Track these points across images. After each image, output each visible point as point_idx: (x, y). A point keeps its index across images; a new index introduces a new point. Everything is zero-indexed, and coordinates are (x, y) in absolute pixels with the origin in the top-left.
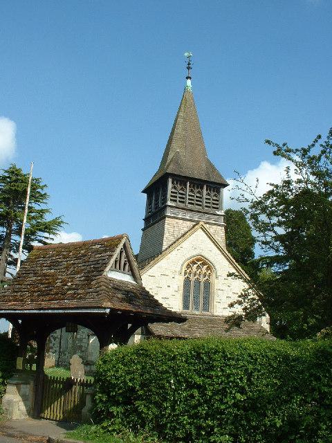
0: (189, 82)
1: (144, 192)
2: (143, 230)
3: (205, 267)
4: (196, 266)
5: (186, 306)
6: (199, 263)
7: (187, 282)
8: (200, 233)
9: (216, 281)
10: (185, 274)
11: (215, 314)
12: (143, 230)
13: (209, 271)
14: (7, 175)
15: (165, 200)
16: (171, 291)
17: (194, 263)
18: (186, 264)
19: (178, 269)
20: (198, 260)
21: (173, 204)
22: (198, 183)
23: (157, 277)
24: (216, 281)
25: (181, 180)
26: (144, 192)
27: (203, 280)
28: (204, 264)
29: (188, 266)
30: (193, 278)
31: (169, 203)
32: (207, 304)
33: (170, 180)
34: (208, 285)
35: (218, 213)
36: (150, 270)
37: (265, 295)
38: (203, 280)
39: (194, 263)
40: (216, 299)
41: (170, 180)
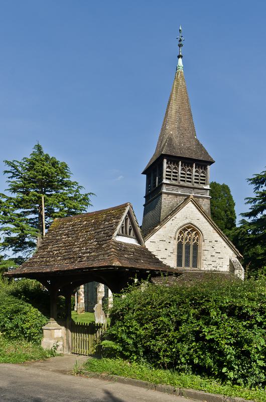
0: (180, 60)
19: (173, 236)
20: (189, 228)
22: (188, 162)
39: (185, 230)
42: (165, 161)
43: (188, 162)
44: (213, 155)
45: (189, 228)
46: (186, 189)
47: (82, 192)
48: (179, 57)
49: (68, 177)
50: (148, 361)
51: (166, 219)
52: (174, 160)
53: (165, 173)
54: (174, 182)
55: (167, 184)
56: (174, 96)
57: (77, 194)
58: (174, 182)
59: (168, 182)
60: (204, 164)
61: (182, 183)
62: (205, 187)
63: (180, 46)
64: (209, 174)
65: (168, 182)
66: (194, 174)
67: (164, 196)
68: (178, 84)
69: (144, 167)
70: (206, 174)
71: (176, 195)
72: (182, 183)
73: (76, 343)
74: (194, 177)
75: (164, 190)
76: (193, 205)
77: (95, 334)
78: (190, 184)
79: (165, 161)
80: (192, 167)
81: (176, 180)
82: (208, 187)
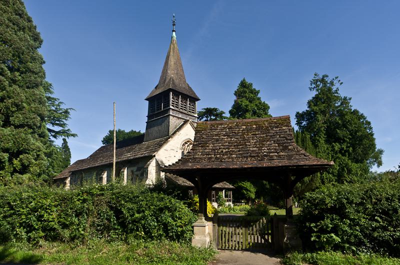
0: (174, 33)
19: (179, 147)
20: (188, 142)
22: (185, 97)
25: (177, 94)
31: (171, 107)
39: (186, 143)
42: (171, 93)
43: (185, 97)
44: (199, 95)
45: (188, 142)
46: (184, 115)
47: (63, 107)
48: (173, 31)
49: (51, 93)
50: (7, 241)
51: (174, 133)
52: (177, 94)
53: (171, 102)
54: (176, 109)
55: (172, 109)
56: (171, 53)
57: (58, 107)
58: (176, 109)
59: (172, 108)
60: (194, 99)
61: (181, 110)
62: (195, 115)
63: (174, 25)
64: (196, 106)
65: (172, 108)
66: (188, 105)
67: (171, 117)
68: (174, 47)
69: (147, 95)
70: (195, 107)
71: (179, 118)
72: (181, 110)
73: (224, 239)
74: (188, 108)
75: (171, 113)
76: (191, 126)
77: (251, 228)
78: (186, 112)
79: (171, 93)
80: (187, 100)
81: (177, 107)
82: (196, 115)
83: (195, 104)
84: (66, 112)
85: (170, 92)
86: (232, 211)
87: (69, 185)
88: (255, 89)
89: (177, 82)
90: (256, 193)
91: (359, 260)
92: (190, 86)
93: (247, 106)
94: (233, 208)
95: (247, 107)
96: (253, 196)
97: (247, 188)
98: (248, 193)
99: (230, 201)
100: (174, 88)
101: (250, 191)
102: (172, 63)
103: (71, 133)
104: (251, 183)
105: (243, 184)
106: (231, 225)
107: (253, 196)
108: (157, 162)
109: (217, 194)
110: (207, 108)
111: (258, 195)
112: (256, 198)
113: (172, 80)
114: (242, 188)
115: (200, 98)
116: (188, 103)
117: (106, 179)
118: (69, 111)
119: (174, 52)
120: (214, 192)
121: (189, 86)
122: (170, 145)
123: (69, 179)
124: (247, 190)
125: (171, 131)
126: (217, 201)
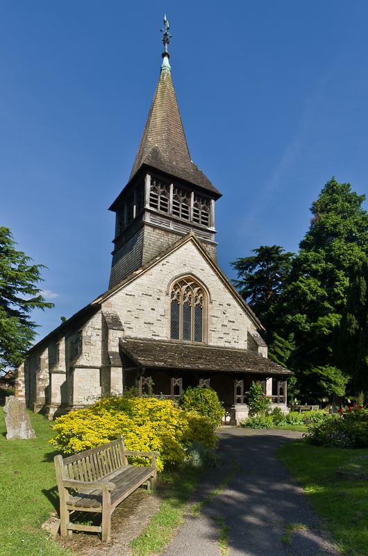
0: (166, 61)
1: (112, 209)
2: (113, 253)
3: (197, 289)
4: (185, 287)
5: (174, 333)
6: (189, 284)
7: (175, 305)
8: (189, 246)
9: (210, 306)
10: (172, 296)
11: (211, 344)
12: (113, 253)
13: (201, 295)
14: (98, 401)
15: (142, 211)
16: (155, 315)
17: (182, 283)
18: (171, 287)
19: (164, 289)
20: (188, 280)
21: (153, 209)
22: (184, 187)
23: (136, 296)
24: (210, 306)
25: (163, 178)
26: (112, 209)
27: (193, 305)
28: (195, 285)
29: (176, 287)
30: (181, 302)
31: (147, 206)
32: (199, 336)
33: (148, 178)
34: (199, 310)
35: (209, 229)
36: (128, 288)
37: (333, 290)
38: (193, 305)
39: (182, 283)
40: (211, 327)
41: (148, 178)
48: (164, 55)
53: (148, 197)
63: (166, 41)
75: (148, 218)
83: (209, 204)
84: (33, 270)
85: (145, 176)
86: (283, 424)
87: (23, 374)
88: (355, 194)
89: (165, 156)
90: (348, 386)
91: (274, 354)
92: (200, 169)
93: (335, 226)
94: (288, 417)
95: (335, 228)
96: (341, 392)
97: (330, 377)
98: (330, 387)
99: (282, 401)
100: (154, 165)
101: (335, 383)
102: (158, 120)
103: (45, 302)
104: (338, 368)
105: (321, 370)
106: (190, 486)
107: (341, 392)
108: (103, 318)
109: (247, 386)
110: (262, 248)
111: (351, 389)
112: (347, 395)
113: (155, 152)
114: (318, 377)
115: (220, 192)
116: (192, 203)
117: (47, 361)
118: (39, 269)
119: (162, 97)
120: (240, 383)
121: (197, 170)
122: (142, 285)
123: (23, 365)
124: (328, 380)
125: (146, 256)
126: (246, 402)
